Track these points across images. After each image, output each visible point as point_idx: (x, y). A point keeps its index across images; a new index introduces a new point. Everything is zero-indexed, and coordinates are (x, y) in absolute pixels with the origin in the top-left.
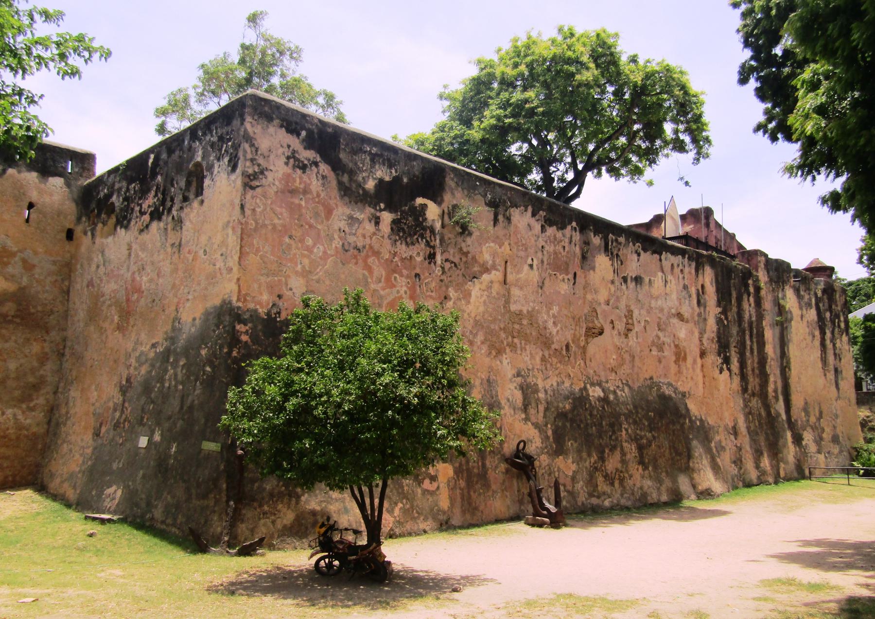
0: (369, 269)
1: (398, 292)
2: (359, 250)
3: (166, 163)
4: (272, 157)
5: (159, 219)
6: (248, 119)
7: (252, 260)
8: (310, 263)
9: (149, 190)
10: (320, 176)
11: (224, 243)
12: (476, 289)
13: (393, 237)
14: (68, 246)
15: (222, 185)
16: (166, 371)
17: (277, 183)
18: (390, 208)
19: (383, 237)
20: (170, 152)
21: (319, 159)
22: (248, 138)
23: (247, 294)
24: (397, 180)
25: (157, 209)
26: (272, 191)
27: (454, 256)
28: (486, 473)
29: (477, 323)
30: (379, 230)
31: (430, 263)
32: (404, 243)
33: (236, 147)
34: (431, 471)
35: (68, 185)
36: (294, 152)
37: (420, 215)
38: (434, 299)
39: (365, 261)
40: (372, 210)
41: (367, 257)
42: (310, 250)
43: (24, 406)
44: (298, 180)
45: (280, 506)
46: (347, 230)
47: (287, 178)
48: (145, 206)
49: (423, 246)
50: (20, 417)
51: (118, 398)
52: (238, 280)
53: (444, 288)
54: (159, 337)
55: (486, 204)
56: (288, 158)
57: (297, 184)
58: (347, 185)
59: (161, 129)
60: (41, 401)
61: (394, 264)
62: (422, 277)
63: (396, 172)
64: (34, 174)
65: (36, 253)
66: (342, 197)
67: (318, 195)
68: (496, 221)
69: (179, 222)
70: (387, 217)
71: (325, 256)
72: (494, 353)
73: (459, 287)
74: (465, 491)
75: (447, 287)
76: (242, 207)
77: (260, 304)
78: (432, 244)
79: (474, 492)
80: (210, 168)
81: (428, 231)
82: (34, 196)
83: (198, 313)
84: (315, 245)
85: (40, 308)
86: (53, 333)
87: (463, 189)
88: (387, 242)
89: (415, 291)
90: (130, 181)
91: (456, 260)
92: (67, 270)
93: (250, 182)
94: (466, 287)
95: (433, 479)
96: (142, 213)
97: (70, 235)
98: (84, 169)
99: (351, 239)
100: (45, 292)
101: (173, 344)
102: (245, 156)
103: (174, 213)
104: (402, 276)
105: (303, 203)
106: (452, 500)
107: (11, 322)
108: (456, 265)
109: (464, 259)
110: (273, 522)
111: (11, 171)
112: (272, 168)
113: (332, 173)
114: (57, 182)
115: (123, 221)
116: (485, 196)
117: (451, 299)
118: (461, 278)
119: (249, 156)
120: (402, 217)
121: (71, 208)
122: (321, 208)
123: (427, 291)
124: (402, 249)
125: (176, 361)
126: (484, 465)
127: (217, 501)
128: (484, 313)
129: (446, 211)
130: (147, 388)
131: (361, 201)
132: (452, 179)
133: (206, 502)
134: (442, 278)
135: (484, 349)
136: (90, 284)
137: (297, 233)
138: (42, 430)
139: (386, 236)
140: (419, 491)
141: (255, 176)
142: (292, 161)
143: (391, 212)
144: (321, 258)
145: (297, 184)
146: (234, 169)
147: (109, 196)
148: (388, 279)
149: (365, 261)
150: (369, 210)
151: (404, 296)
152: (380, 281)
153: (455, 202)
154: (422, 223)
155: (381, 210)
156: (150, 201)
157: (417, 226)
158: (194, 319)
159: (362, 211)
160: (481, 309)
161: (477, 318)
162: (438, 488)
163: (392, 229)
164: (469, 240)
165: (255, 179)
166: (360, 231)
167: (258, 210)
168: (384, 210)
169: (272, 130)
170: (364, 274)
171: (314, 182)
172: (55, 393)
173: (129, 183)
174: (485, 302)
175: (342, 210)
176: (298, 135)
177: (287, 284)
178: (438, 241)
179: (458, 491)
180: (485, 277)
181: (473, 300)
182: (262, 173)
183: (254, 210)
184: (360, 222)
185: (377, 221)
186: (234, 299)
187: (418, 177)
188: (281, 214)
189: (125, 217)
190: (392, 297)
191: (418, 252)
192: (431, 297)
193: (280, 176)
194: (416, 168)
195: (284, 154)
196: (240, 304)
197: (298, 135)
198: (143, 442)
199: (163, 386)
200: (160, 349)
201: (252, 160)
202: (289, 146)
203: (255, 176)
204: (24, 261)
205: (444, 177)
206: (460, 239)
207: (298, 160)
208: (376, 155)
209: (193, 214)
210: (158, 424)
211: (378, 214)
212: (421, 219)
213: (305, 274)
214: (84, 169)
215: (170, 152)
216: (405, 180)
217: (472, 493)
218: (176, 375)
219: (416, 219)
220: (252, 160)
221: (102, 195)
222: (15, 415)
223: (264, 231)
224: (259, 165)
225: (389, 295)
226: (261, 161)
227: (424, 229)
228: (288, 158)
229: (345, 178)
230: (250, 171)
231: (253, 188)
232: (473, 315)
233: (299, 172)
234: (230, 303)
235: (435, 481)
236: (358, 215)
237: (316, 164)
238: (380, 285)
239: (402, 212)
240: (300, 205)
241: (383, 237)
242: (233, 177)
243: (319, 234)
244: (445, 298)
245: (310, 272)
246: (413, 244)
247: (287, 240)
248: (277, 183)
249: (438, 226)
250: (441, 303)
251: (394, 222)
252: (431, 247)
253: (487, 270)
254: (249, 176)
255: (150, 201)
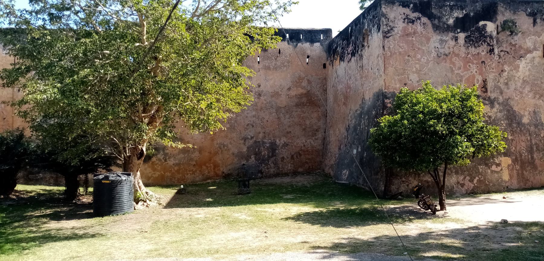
0: (454, 64)
1: (471, 72)
2: (447, 55)
3: (355, 31)
4: (396, 21)
5: (354, 56)
6: (383, 6)
7: (391, 70)
8: (420, 66)
9: (350, 43)
10: (422, 24)
11: (378, 64)
12: (523, 64)
13: (467, 45)
14: (324, 71)
15: (375, 39)
16: (361, 121)
17: (400, 32)
18: (463, 30)
19: (460, 46)
20: (356, 25)
21: (420, 16)
22: (384, 15)
23: (389, 86)
24: (466, 15)
25: (353, 52)
26: (397, 37)
27: (506, 48)
28: (534, 161)
29: (524, 81)
30: (458, 43)
31: (490, 54)
32: (473, 47)
33: (379, 20)
34: (497, 161)
35: (322, 45)
36: (407, 15)
37: (483, 30)
38: (494, 73)
39: (451, 60)
40: (453, 34)
41: (452, 57)
42: (419, 60)
43: (313, 138)
44: (410, 29)
45: (410, 179)
46: (439, 46)
47: (404, 29)
48: (349, 51)
49: (485, 46)
50: (312, 143)
51: (346, 134)
52: (384, 80)
53: (501, 66)
54: (358, 107)
55: (527, 15)
56: (404, 19)
57: (410, 30)
58: (437, 24)
59: (361, 8)
60: (320, 136)
61: (468, 59)
62: (486, 62)
63: (466, 11)
64: (308, 44)
65: (312, 76)
66: (435, 31)
67: (422, 33)
68: (535, 22)
69: (361, 56)
70: (462, 36)
71: (428, 62)
72: (538, 96)
73: (510, 64)
74: (520, 172)
75: (503, 65)
76: (383, 47)
77: (395, 89)
78: (491, 44)
79: (526, 172)
80: (370, 31)
81: (488, 38)
82: (309, 52)
83: (371, 95)
84: (422, 57)
85: (316, 98)
86: (322, 108)
87: (510, 11)
88: (463, 49)
89: (482, 70)
90: (343, 40)
91: (508, 50)
92: (324, 80)
93: (386, 35)
94: (517, 63)
95: (498, 165)
96: (348, 54)
97: (324, 66)
98: (327, 36)
99: (442, 51)
100: (317, 91)
101: (363, 109)
102: (383, 24)
103: (359, 52)
104: (473, 64)
105: (414, 39)
106: (511, 176)
107: (306, 105)
108: (508, 53)
109: (513, 48)
110: (408, 186)
111: (299, 44)
112: (396, 26)
113: (429, 21)
114: (317, 44)
115: (342, 59)
116: (526, 11)
117: (506, 71)
118: (512, 59)
119: (385, 23)
120: (471, 34)
121: (324, 55)
122: (424, 39)
123: (490, 69)
124: (472, 50)
125: (364, 117)
126: (532, 157)
127: (382, 176)
128: (529, 75)
129: (499, 25)
130: (355, 129)
131: (446, 31)
132: (503, 7)
133: (377, 177)
134: (499, 61)
135: (531, 95)
136: (333, 86)
137: (412, 53)
138: (320, 148)
139: (462, 45)
140: (489, 171)
141: (389, 32)
142: (406, 20)
143: (464, 33)
144: (425, 63)
145: (410, 30)
146: (379, 31)
147: (336, 48)
148: (465, 67)
149: (451, 60)
150: (451, 34)
151: (475, 74)
152: (460, 69)
153: (505, 19)
154: (484, 34)
155: (458, 33)
156: (351, 48)
157: (481, 37)
158: (370, 98)
159: (447, 36)
160: (527, 73)
161: (525, 79)
162: (502, 170)
163: (465, 41)
164: (516, 38)
165: (388, 33)
166: (447, 45)
167: (391, 47)
168: (460, 32)
169: (395, 8)
170: (450, 67)
171: (419, 27)
172: (325, 132)
173: (343, 41)
174: (529, 70)
175: (435, 38)
176: (409, 7)
177: (408, 78)
178: (495, 42)
179: (515, 171)
180: (529, 56)
181: (520, 69)
182: (392, 29)
183: (389, 47)
184: (446, 41)
185: (456, 39)
186: (384, 88)
187: (479, 11)
188: (403, 46)
189: (343, 56)
190: (468, 76)
191: (483, 50)
192: (492, 72)
193: (401, 28)
194: (478, 7)
195: (402, 18)
196: (386, 91)
197: (409, 7)
198: (355, 151)
199: (360, 128)
200: (358, 112)
201: (386, 25)
202: (404, 14)
203: (389, 32)
204: (308, 80)
205: (497, 7)
206: (510, 38)
207: (410, 19)
208: (453, 5)
209: (366, 53)
210: (360, 144)
211: (456, 35)
212: (483, 33)
213: (418, 72)
214: (327, 36)
215: (356, 25)
216: (472, 14)
217: (524, 172)
218: (364, 123)
219: (480, 33)
220: (386, 25)
221: (334, 47)
222: (310, 142)
223: (395, 56)
224: (390, 26)
225: (466, 74)
226: (391, 24)
227: (486, 37)
228: (404, 19)
229: (436, 22)
230: (386, 30)
231: (387, 37)
232: (521, 78)
233: (410, 24)
234: (382, 90)
235: (499, 166)
236: (444, 38)
237: (419, 18)
238: (460, 70)
239: (471, 31)
240: (412, 40)
241: (460, 46)
242: (379, 34)
243: (424, 52)
244: (502, 71)
245: (420, 70)
246: (479, 46)
247: (407, 58)
248: (400, 32)
249: (495, 34)
250: (500, 74)
251: (466, 37)
252: (490, 46)
253: (529, 51)
254: (385, 32)
255: (351, 48)
